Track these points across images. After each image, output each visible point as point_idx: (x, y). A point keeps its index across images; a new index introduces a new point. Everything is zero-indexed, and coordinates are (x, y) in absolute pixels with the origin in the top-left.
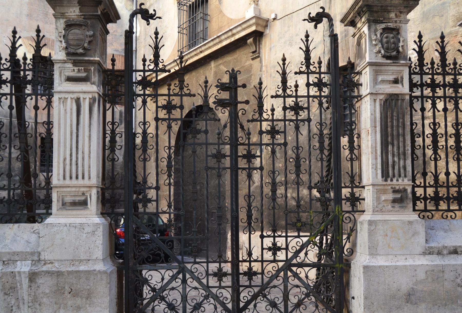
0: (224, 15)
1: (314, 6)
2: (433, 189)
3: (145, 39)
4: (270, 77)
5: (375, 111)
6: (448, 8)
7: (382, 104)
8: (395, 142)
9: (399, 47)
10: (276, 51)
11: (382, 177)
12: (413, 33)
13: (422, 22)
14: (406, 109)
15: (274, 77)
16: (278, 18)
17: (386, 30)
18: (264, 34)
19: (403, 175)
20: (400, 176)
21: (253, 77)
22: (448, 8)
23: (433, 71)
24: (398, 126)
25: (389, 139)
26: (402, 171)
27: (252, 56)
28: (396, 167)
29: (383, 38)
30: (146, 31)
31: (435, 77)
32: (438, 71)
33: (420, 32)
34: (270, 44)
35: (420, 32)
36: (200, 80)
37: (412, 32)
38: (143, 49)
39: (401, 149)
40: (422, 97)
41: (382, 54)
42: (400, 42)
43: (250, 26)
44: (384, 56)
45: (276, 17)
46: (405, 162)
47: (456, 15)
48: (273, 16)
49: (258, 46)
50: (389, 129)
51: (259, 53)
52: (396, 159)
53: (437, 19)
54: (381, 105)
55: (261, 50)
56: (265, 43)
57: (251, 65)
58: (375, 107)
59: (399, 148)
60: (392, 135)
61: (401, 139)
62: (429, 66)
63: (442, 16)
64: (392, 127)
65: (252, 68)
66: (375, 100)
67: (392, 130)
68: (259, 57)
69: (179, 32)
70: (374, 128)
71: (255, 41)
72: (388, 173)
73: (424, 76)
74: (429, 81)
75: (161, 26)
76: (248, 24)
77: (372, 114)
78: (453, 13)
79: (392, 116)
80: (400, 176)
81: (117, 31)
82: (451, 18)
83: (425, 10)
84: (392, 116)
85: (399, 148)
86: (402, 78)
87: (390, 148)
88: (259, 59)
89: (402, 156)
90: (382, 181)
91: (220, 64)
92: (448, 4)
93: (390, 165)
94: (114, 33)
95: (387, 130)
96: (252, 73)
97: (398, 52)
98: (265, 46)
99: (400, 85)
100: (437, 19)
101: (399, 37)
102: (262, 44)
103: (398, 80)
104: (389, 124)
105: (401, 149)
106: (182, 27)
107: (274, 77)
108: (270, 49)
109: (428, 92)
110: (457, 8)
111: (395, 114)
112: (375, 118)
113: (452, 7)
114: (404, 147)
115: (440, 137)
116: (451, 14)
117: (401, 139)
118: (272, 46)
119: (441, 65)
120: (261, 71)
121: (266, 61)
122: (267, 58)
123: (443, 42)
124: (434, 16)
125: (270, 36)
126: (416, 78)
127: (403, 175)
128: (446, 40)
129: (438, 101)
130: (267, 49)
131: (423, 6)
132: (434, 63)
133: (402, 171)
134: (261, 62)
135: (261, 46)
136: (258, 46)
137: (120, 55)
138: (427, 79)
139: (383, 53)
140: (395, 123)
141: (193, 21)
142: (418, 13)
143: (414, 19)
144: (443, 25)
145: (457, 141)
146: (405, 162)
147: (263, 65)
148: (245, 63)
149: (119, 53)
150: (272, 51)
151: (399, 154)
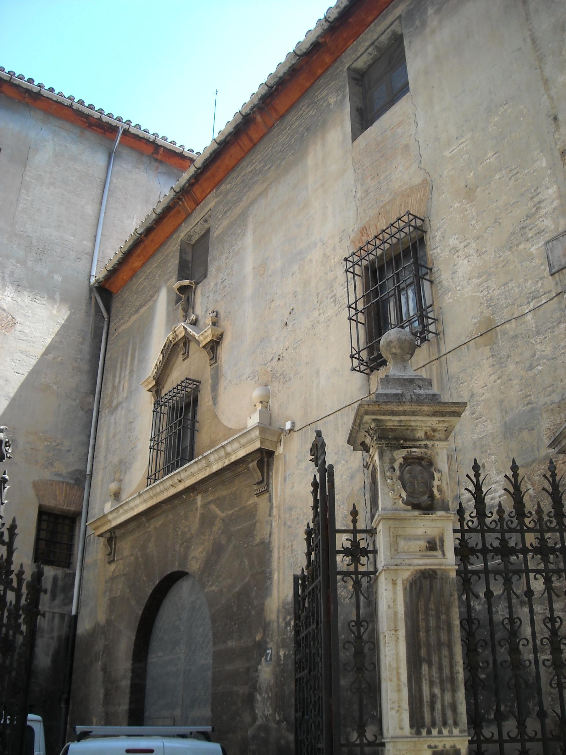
0: (219, 421)
1: (349, 411)
2: (518, 746)
3: (105, 457)
4: (284, 526)
5: (394, 601)
6: (540, 417)
7: (408, 588)
8: (435, 659)
9: (433, 487)
10: (293, 483)
11: (411, 727)
12: (493, 457)
13: (505, 438)
14: (452, 595)
15: (290, 527)
16: (296, 429)
17: (408, 461)
18: (276, 454)
19: (450, 721)
20: (445, 724)
21: (258, 524)
22: (540, 417)
23: (502, 526)
24: (438, 628)
25: (423, 652)
26: (449, 713)
27: (257, 490)
28: (438, 706)
29: (405, 472)
30: (108, 445)
31: (507, 535)
32: (513, 526)
33: (475, 460)
34: (285, 471)
35: (475, 460)
36: (179, 528)
37: (492, 455)
38: (101, 473)
39: (446, 671)
40: (486, 571)
41: (403, 499)
42: (434, 479)
43: (252, 441)
44: (407, 503)
45: (294, 427)
46: (453, 696)
47: (552, 428)
48: (288, 426)
49: (265, 474)
50: (422, 634)
51: (268, 485)
52: (437, 691)
53: (525, 433)
54: (405, 589)
55: (271, 481)
56: (277, 469)
57: (255, 505)
58: (395, 593)
59: (440, 668)
60: (428, 645)
61: (445, 652)
62: (495, 517)
63: (533, 429)
64: (428, 630)
65: (256, 510)
66: (394, 583)
67: (428, 636)
68: (267, 491)
69: (151, 448)
70: (393, 632)
71: (260, 465)
72: (423, 718)
73: (487, 535)
74: (496, 544)
75: (129, 437)
76: (249, 437)
77: (389, 607)
78: (547, 425)
79: (427, 609)
80: (434, 724)
81: (62, 444)
82: (545, 433)
83: (507, 420)
84: (427, 609)
85: (440, 668)
86: (442, 541)
87: (425, 668)
88: (267, 495)
89: (448, 686)
90: (411, 733)
91: (210, 502)
92: (538, 412)
93: (425, 703)
94: (59, 447)
95: (418, 636)
96: (257, 519)
97: (432, 496)
98: (277, 473)
99: (439, 553)
100: (525, 433)
101: (433, 470)
102: (272, 470)
103: (435, 544)
104: (422, 624)
105: (446, 671)
106: (156, 439)
107: (290, 527)
108: (285, 479)
109: (496, 562)
110: (552, 418)
111: (432, 606)
112: (396, 614)
113: (544, 416)
114: (452, 667)
115: (523, 645)
116: (545, 427)
117: (445, 652)
118: (288, 474)
119: (517, 514)
120: (270, 515)
121: (278, 499)
122: (279, 494)
123: (515, 475)
124: (520, 430)
125: (285, 457)
126: (474, 540)
127: (450, 721)
128: (521, 472)
129: (515, 578)
130: (280, 479)
131: (504, 413)
132: (503, 512)
133: (449, 713)
134: (270, 500)
135: (271, 473)
136: (265, 474)
137: (63, 482)
138: (493, 540)
139: (405, 498)
140: (432, 623)
141: (176, 428)
142: (498, 424)
143: (492, 433)
144: (535, 443)
145: (556, 650)
146: (453, 696)
147: (274, 505)
148: (246, 502)
149: (61, 479)
150: (287, 482)
151: (442, 682)
